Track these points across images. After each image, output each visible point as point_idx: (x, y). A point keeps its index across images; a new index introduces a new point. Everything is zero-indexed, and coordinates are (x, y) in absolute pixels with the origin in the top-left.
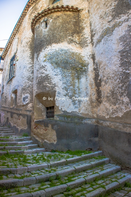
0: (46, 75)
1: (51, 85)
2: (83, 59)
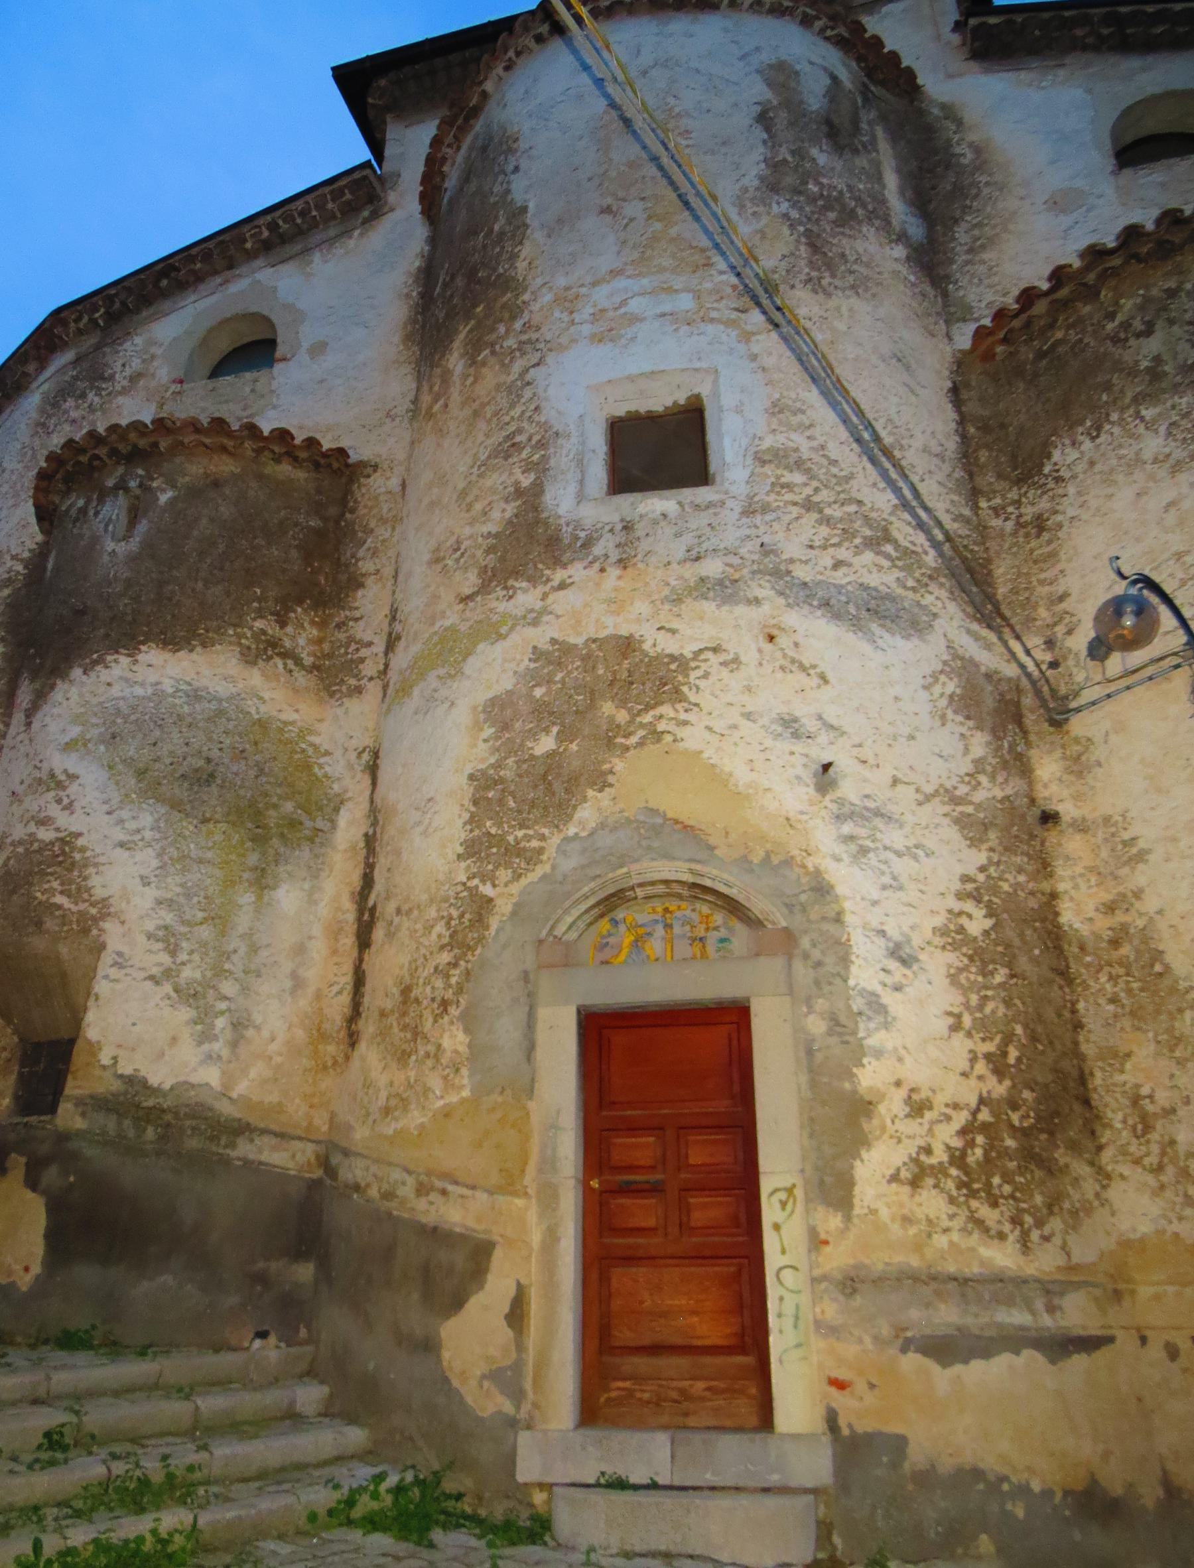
0: (62, 840)
1: (82, 906)
2: (316, 770)
